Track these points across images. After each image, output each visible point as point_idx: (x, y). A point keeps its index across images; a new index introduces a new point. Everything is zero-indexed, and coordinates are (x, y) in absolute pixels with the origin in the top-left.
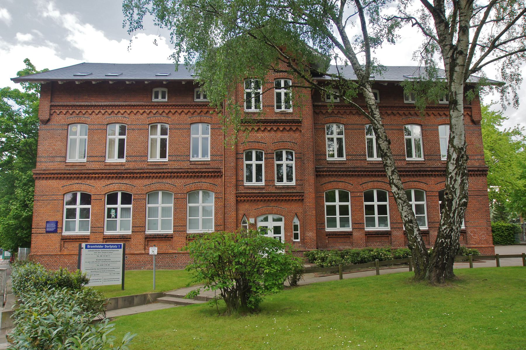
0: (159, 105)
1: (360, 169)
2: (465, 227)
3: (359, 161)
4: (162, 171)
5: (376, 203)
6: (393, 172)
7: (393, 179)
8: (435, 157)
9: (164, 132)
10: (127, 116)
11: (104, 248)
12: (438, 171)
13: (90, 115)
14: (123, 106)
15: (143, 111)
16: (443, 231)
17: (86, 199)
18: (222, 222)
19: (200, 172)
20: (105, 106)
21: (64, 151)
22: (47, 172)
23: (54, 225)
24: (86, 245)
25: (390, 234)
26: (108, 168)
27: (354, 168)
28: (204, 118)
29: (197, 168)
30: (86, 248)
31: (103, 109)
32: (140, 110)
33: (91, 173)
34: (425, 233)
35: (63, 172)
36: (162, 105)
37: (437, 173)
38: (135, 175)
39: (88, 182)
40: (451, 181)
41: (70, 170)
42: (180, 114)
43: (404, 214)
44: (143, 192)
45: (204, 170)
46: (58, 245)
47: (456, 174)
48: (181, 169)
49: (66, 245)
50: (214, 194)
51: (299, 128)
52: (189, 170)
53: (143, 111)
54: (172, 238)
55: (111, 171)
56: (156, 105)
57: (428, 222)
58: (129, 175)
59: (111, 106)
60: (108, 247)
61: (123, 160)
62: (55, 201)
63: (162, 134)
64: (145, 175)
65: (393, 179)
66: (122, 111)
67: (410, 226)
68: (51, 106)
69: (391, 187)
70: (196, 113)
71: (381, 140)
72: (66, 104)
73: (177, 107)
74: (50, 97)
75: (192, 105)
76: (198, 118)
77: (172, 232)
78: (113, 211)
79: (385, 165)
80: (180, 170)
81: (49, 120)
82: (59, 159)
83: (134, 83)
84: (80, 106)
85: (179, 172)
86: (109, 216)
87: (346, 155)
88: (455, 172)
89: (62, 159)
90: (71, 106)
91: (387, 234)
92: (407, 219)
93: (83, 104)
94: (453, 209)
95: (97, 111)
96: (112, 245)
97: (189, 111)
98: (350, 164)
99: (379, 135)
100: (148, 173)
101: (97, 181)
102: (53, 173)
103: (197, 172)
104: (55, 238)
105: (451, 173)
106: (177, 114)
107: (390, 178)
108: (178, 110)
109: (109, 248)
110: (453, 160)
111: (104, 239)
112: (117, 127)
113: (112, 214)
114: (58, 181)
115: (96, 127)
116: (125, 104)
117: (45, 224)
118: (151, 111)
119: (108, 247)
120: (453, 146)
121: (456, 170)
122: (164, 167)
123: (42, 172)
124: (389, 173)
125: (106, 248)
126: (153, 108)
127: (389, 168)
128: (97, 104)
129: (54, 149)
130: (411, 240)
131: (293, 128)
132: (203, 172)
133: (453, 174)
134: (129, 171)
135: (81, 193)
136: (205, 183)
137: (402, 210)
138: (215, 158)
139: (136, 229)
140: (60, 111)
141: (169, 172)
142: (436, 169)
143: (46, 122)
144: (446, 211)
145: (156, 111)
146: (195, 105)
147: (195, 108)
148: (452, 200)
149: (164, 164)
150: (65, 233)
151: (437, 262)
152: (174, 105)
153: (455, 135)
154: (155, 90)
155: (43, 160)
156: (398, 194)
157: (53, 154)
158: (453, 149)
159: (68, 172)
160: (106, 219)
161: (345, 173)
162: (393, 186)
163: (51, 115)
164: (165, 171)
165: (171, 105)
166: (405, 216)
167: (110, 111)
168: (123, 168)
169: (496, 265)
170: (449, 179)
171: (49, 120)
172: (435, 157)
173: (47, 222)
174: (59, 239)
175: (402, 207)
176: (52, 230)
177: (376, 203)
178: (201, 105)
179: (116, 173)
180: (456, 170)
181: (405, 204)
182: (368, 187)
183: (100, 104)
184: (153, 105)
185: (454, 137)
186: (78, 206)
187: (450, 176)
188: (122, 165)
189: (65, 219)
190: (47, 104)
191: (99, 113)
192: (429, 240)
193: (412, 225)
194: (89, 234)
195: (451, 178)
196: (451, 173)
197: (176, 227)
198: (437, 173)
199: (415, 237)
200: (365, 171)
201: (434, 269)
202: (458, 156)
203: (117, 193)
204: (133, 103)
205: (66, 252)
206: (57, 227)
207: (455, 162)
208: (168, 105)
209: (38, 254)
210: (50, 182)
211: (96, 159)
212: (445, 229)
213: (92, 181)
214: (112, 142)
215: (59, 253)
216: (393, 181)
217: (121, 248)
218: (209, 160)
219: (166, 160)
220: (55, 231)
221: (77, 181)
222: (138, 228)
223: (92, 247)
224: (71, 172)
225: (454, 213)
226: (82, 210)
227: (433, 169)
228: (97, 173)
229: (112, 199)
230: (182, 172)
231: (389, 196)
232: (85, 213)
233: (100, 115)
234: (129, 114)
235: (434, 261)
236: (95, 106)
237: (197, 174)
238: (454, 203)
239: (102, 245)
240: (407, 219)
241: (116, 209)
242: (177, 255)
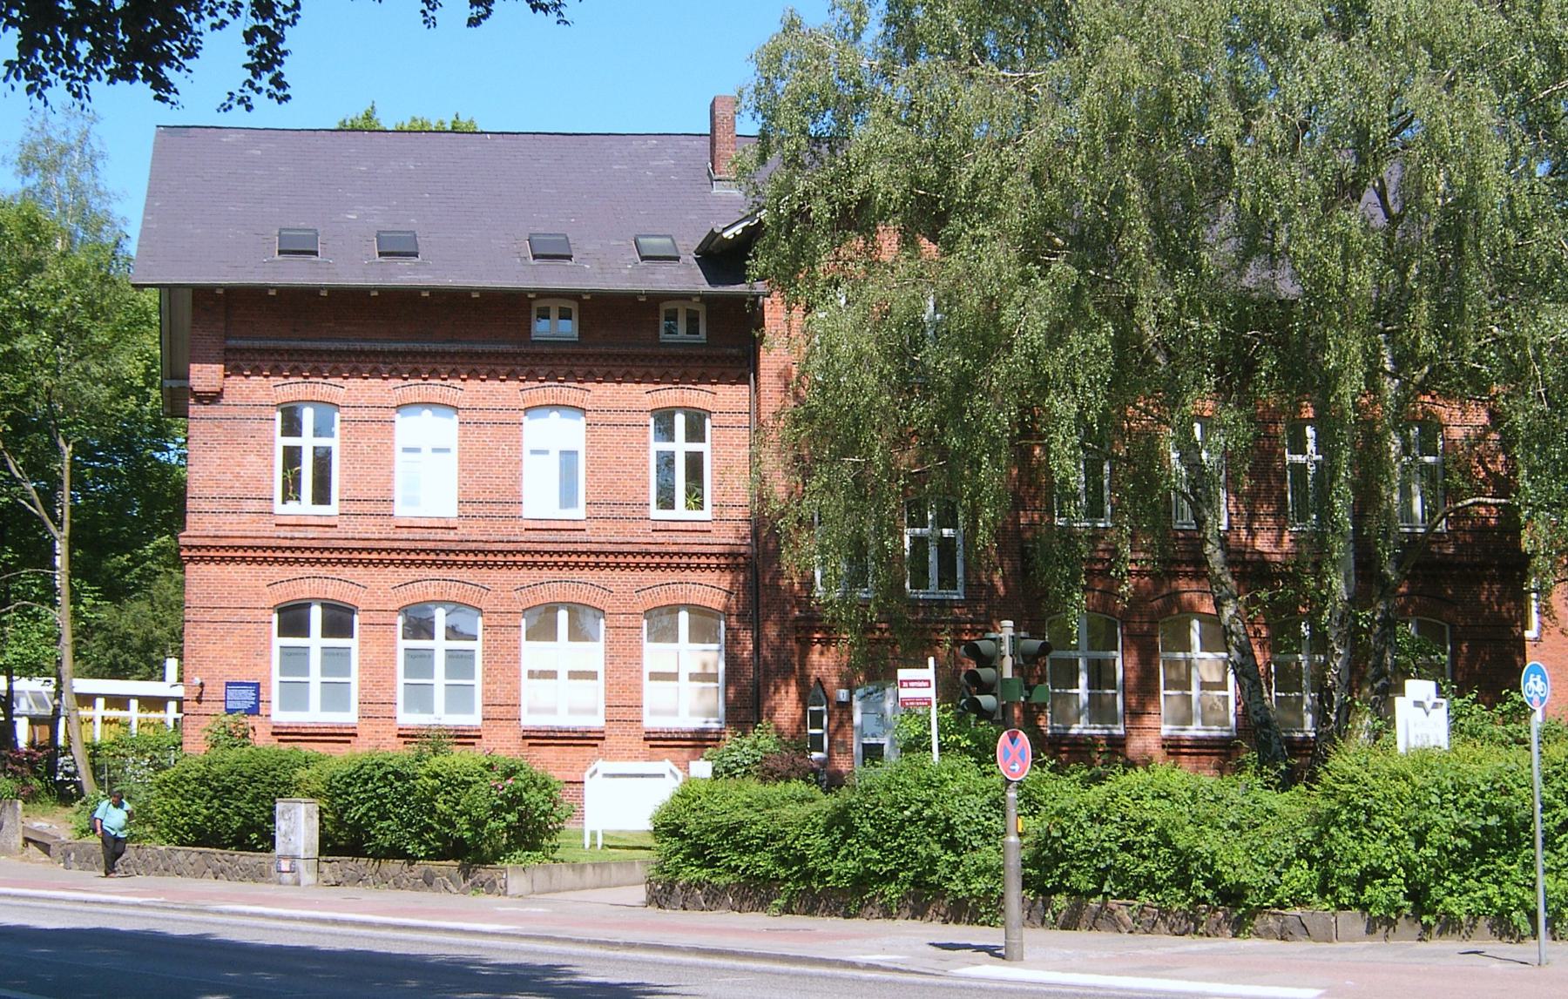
22: (223, 543)
23: (249, 694)
39: (347, 572)
52: (653, 548)
93: (324, 345)
129: (238, 476)
134: (473, 546)
139: (495, 712)
173: (228, 684)
206: (258, 701)
211: (367, 507)
229: (293, 619)
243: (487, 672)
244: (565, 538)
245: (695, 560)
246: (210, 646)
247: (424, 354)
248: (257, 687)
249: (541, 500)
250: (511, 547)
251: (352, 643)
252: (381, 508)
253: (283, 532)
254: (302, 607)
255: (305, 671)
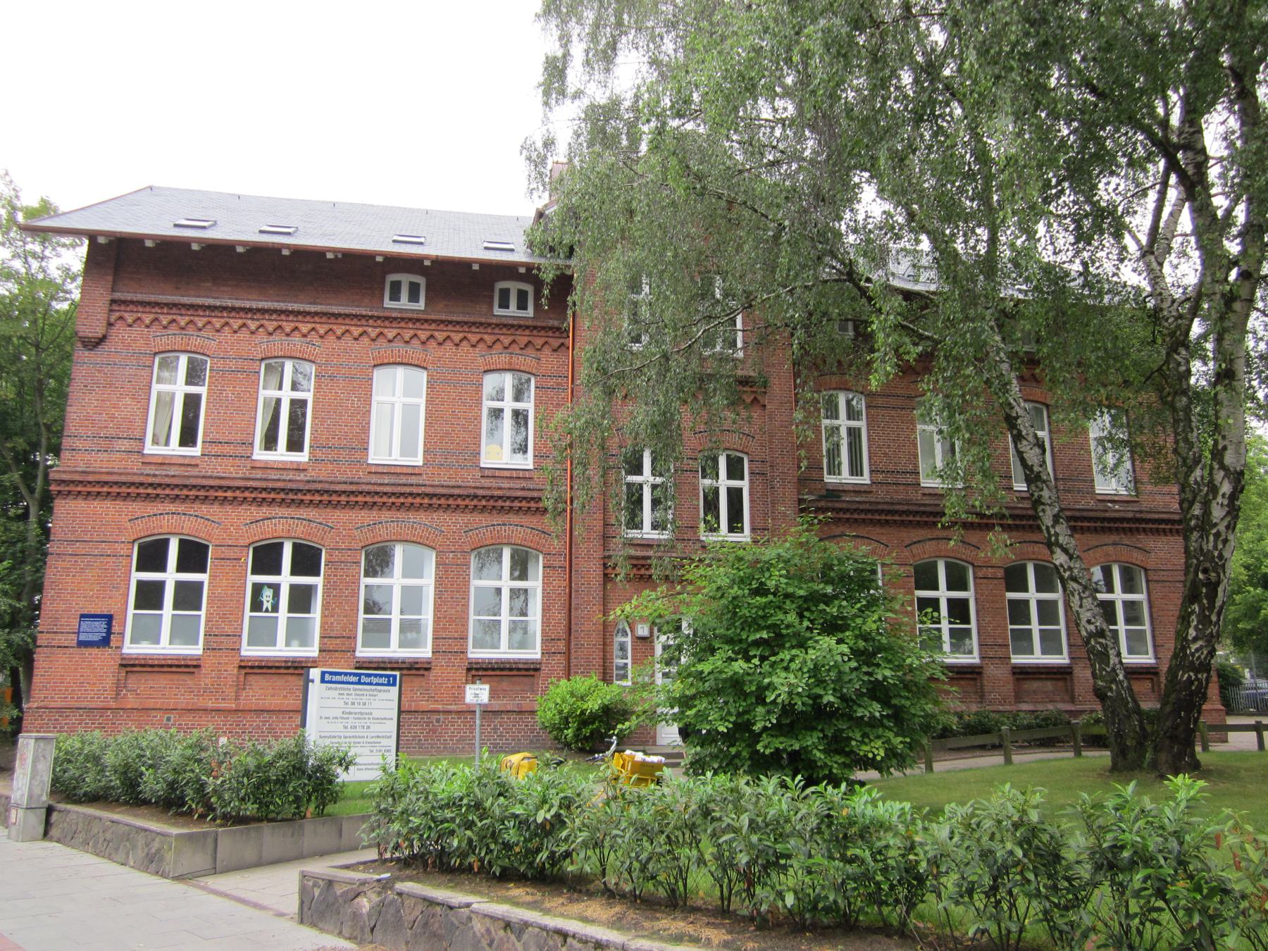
0: (403, 319)
1: (905, 508)
2: (1156, 658)
3: (901, 488)
4: (408, 490)
5: (943, 594)
6: (1056, 519)
7: (1057, 535)
8: (1080, 485)
9: (194, 376)
10: (318, 341)
11: (359, 683)
12: (1089, 519)
13: (218, 331)
14: (309, 313)
15: (361, 330)
16: (1193, 655)
17: (193, 557)
18: (561, 631)
19: (508, 498)
20: (258, 310)
21: (139, 422)
22: (90, 478)
23: (101, 626)
24: (323, 674)
25: (980, 673)
26: (259, 475)
27: (892, 504)
28: (519, 361)
29: (500, 488)
30: (323, 681)
31: (253, 319)
32: (352, 328)
33: (212, 487)
34: (1062, 673)
35: (137, 479)
36: (410, 319)
37: (1086, 524)
38: (335, 498)
39: (204, 509)
40: (1216, 541)
41: (155, 475)
42: (457, 345)
43: (1085, 616)
44: (354, 545)
45: (519, 494)
46: (109, 682)
47: (1227, 527)
48: (459, 487)
49: (133, 681)
50: (433, 556)
51: (759, 398)
52: (481, 492)
53: (361, 330)
54: (427, 669)
55: (270, 485)
56: (395, 319)
57: (1070, 646)
58: (317, 498)
59: (275, 311)
60: (367, 680)
61: (303, 457)
62: (109, 559)
63: (189, 382)
64: (360, 498)
65: (1057, 535)
66: (305, 328)
67: (1101, 644)
68: (113, 301)
69: (1052, 552)
70: (498, 345)
71: (1025, 442)
72: (152, 298)
73: (450, 328)
74: (110, 278)
75: (490, 325)
76: (504, 359)
77: (430, 655)
78: (267, 594)
79: (1038, 502)
80: (456, 491)
81: (103, 339)
82: (124, 445)
83: (340, 256)
84: (192, 306)
85: (452, 496)
86: (257, 605)
87: (871, 472)
88: (1225, 523)
89: (134, 445)
90: (166, 305)
91: (972, 673)
92: (1092, 628)
93: (199, 301)
94: (1218, 604)
95: (236, 324)
96: (376, 676)
97: (481, 339)
98: (881, 495)
99: (1020, 432)
100: (369, 493)
101: (229, 508)
102: (106, 483)
103: (500, 497)
104: (103, 660)
105: (1216, 525)
106: (448, 345)
107: (1048, 532)
108: (452, 335)
109: (371, 684)
110: (1223, 495)
111: (241, 667)
112: (183, 361)
113: (264, 599)
114: (120, 504)
115: (233, 365)
116: (313, 308)
117: (75, 623)
118: (448, 337)
119: (367, 680)
120: (1223, 467)
121: (1228, 519)
122: (413, 480)
123: (77, 477)
124: (1047, 520)
125: (364, 684)
126: (387, 323)
127: (1047, 508)
128: (238, 304)
129: (113, 417)
130: (1102, 678)
131: (744, 397)
132: (516, 498)
133: (1222, 527)
134: (319, 487)
135: (181, 540)
136: (518, 528)
137: (1081, 606)
138: (880, 477)
139: (331, 644)
140: (136, 315)
141: (427, 495)
142: (1085, 514)
143: (95, 343)
144: (1202, 609)
145: (395, 332)
146: (497, 325)
147: (497, 331)
148: (1218, 583)
149: (189, 464)
150: (131, 649)
151: (1175, 728)
152: (442, 322)
153: (1226, 443)
154: (392, 277)
155: (78, 444)
156: (1070, 569)
157: (112, 432)
158: (1222, 473)
159: (151, 480)
160: (248, 613)
161: (870, 516)
162: (1058, 550)
163: (110, 325)
164: (415, 490)
165: (434, 321)
166: (1089, 622)
167: (271, 326)
168: (302, 477)
169: (1255, 747)
170: (1211, 538)
171: (103, 339)
172: (1080, 485)
173: (82, 616)
174: (113, 664)
175: (1081, 599)
176: (96, 638)
177: (943, 594)
178: (513, 326)
179: (283, 490)
180: (1228, 519)
181: (1087, 593)
182: (924, 552)
183: (247, 304)
184: (387, 318)
185: (1225, 448)
186: (171, 577)
187: (1214, 531)
188: (299, 469)
189: (131, 610)
190: (102, 296)
191: (240, 327)
192: (1073, 691)
193: (1103, 641)
194: (200, 652)
195: (1217, 535)
196: (1216, 525)
197: (441, 642)
198: (1086, 524)
199: (1114, 670)
200: (917, 512)
201: (1167, 742)
202: (1235, 489)
203: (281, 545)
204: (335, 310)
205: (131, 701)
206: (109, 631)
207: (1226, 502)
208: (426, 321)
209: (53, 705)
210: (97, 506)
211: (228, 449)
212: (1197, 650)
213: (216, 508)
214: (166, 402)
215: (113, 705)
216: (1057, 540)
217: (394, 684)
218: (421, 464)
219: (196, 451)
220: (105, 642)
221: (172, 507)
222: (338, 641)
223: (335, 678)
224: (156, 480)
225: (1219, 614)
226: (180, 585)
227: (1077, 514)
228: (229, 488)
229: (267, 559)
230: (459, 496)
231: (975, 578)
232: (188, 597)
233: (244, 334)
234: (321, 337)
235: (1168, 724)
236: (233, 309)
237: (500, 503)
238: (1220, 590)
239: (355, 675)
240: (1092, 628)
241: (276, 588)
242: (441, 717)
243: (325, 607)
244: (404, 481)
245: (516, 504)
246: (69, 579)
247: (288, 313)
248: (109, 618)
249: (500, 453)
250: (353, 488)
251: (317, 581)
252: (240, 450)
253: (148, 470)
254: (163, 545)
255: (159, 606)
